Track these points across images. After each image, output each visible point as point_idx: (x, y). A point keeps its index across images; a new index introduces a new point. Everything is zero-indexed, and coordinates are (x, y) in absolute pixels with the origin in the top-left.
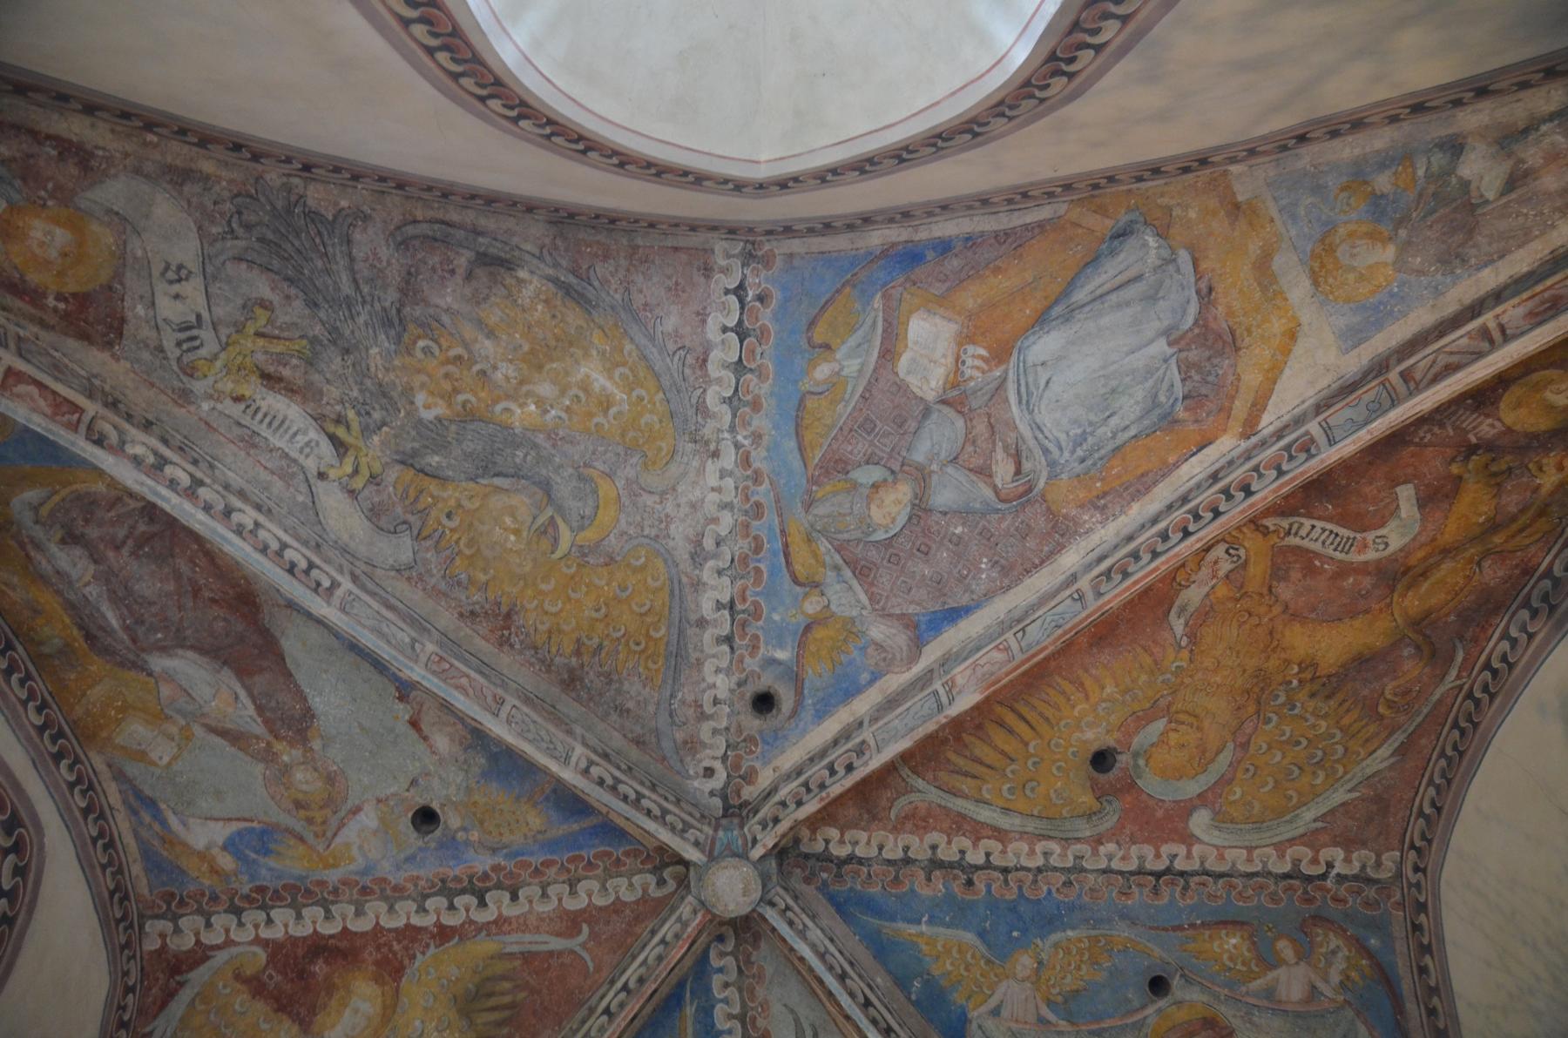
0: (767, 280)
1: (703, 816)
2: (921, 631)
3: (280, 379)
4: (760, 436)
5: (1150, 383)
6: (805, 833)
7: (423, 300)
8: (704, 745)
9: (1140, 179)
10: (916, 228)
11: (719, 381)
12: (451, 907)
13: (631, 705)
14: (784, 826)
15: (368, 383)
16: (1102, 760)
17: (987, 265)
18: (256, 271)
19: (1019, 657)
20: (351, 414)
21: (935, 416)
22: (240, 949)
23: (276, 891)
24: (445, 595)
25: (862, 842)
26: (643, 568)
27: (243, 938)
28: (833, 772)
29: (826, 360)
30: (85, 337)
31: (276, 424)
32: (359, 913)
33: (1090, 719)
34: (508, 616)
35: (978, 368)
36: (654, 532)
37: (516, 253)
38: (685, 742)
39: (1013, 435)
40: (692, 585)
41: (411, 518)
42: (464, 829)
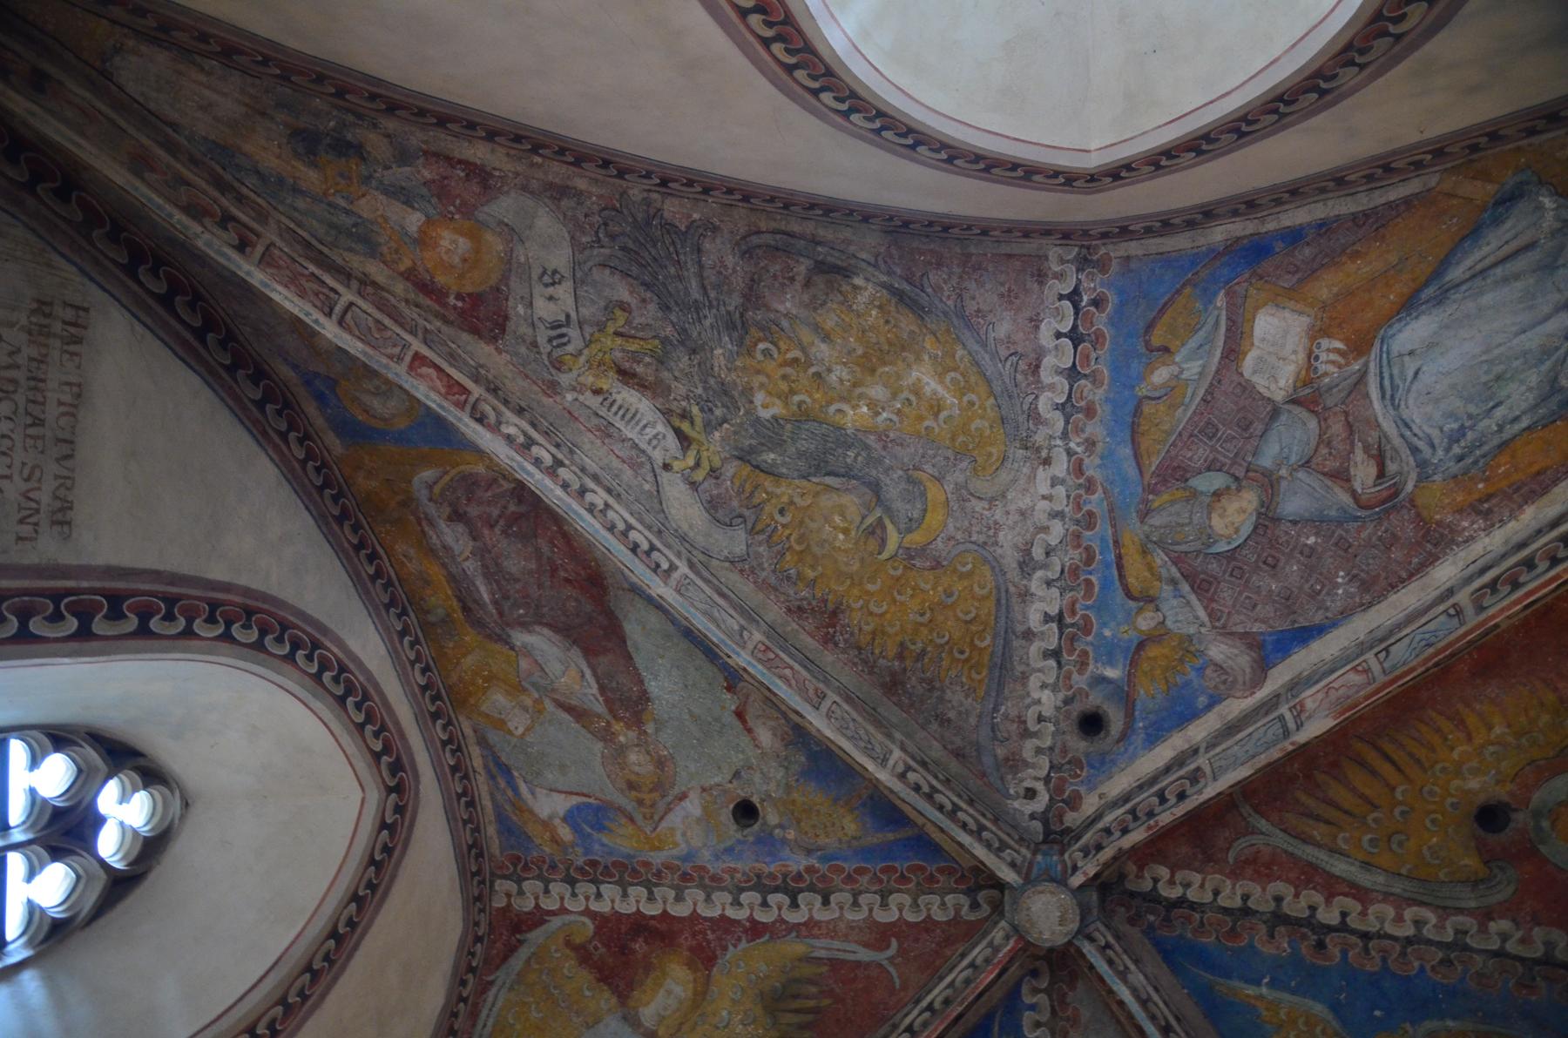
0: (1102, 285)
1: (1022, 839)
2: (1268, 651)
3: (634, 375)
4: (1094, 444)
5: (1548, 364)
6: (1131, 868)
7: (765, 305)
8: (1027, 764)
9: (1532, 132)
10: (1262, 220)
11: (1052, 387)
12: (765, 904)
13: (952, 715)
14: (1107, 854)
15: (712, 381)
16: (1490, 816)
17: (1344, 251)
18: (617, 277)
19: (1382, 679)
20: (695, 410)
21: (1283, 418)
22: (573, 918)
23: (606, 867)
24: (775, 589)
25: (1197, 886)
26: (970, 574)
27: (575, 907)
28: (1163, 799)
29: (1164, 364)
30: (475, 331)
31: (628, 416)
32: (679, 898)
33: (1475, 764)
34: (834, 614)
35: (1333, 362)
36: (982, 538)
37: (853, 262)
38: (1007, 759)
39: (1375, 434)
40: (1020, 595)
41: (747, 513)
42: (781, 826)
